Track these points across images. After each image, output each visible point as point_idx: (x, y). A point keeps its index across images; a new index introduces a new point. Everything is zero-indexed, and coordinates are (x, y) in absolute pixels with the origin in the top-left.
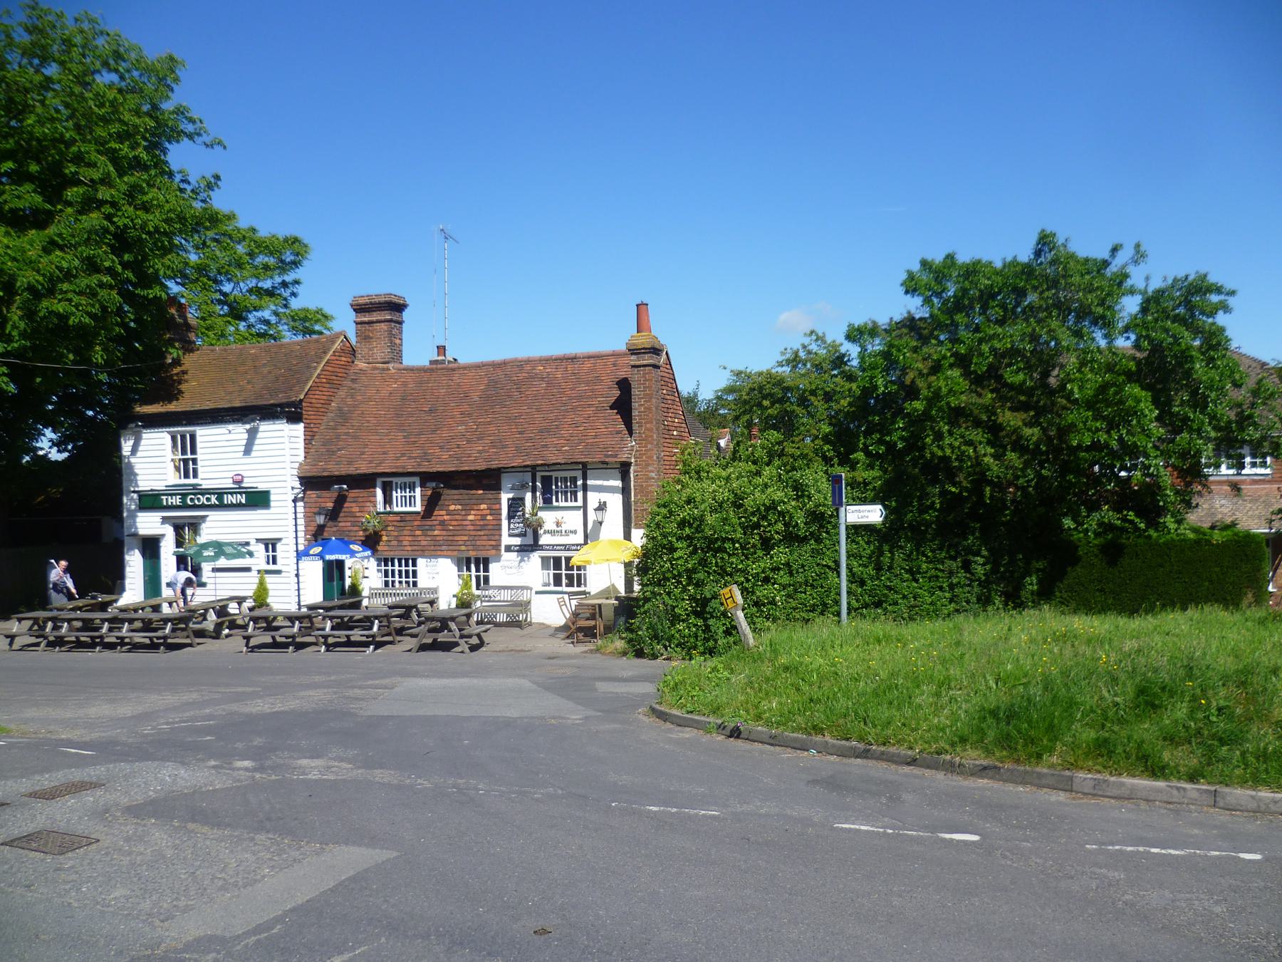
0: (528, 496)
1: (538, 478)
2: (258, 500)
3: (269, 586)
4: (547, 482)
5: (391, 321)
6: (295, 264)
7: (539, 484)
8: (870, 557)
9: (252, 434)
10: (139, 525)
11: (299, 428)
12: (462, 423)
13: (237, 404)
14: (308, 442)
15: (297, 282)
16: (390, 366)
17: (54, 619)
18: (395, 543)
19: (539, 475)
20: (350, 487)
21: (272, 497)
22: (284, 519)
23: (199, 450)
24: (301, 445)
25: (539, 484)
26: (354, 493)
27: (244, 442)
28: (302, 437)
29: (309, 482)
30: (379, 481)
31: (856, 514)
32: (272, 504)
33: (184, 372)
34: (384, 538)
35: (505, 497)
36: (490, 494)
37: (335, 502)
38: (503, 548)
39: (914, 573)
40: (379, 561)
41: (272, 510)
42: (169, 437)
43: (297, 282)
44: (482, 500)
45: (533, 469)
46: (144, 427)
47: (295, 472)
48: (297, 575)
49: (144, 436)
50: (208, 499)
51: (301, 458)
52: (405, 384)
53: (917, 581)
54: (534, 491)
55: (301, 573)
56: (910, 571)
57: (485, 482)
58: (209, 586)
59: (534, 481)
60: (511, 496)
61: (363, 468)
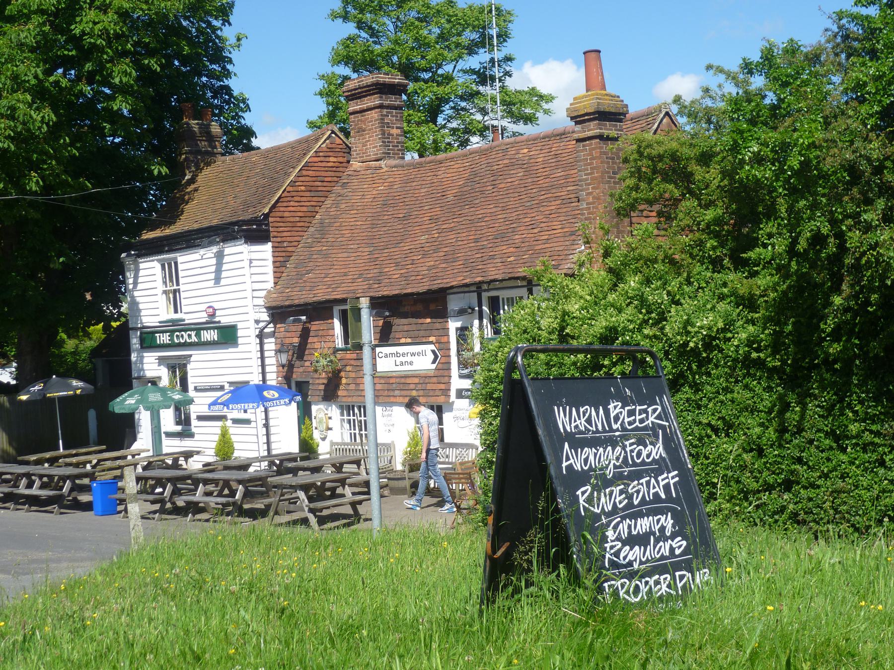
0: (476, 322)
1: (485, 301)
2: (228, 336)
3: (234, 438)
4: (495, 305)
5: (381, 107)
6: (503, 36)
7: (485, 308)
8: (770, 412)
9: (220, 256)
10: (146, 367)
11: (266, 250)
12: (428, 231)
13: (215, 222)
14: (279, 266)
15: (508, 59)
16: (382, 163)
17: (28, 475)
18: (352, 387)
19: (485, 295)
20: (311, 319)
21: (240, 333)
22: (248, 361)
23: (181, 281)
24: (270, 268)
25: (485, 308)
26: (315, 326)
27: (213, 269)
28: (271, 259)
29: (279, 313)
30: (336, 310)
31: (391, 360)
32: (240, 341)
33: (196, 190)
34: (344, 381)
35: (453, 325)
36: (438, 324)
37: (301, 336)
38: (453, 393)
39: (839, 438)
40: (341, 408)
41: (241, 348)
42: (158, 266)
43: (508, 59)
44: (430, 331)
45: (478, 288)
46: (139, 256)
47: (261, 302)
48: (267, 426)
49: (142, 266)
50: (190, 336)
51: (270, 285)
52: (391, 186)
53: (844, 450)
54: (481, 319)
55: (271, 423)
56: (831, 434)
57: (432, 307)
58: (197, 437)
59: (480, 306)
60: (459, 324)
61: (321, 294)
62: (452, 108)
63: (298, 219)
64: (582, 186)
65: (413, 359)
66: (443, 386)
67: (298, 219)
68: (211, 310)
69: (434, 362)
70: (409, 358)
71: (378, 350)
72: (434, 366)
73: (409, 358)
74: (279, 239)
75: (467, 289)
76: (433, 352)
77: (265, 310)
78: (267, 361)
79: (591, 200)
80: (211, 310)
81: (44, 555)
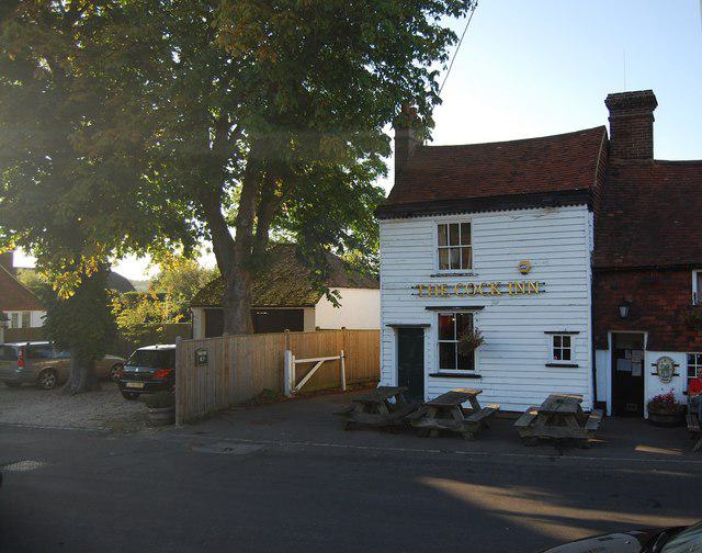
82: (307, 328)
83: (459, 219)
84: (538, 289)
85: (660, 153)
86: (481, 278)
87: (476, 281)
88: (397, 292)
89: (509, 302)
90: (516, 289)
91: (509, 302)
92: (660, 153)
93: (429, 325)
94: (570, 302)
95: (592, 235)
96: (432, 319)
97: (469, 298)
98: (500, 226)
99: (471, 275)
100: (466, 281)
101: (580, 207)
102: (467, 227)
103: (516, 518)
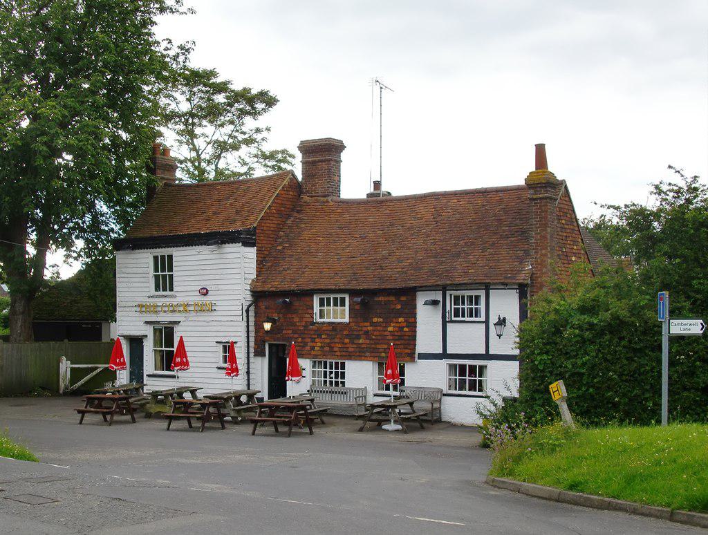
24: (254, 265)
62: (45, 143)
63: (271, 232)
64: (532, 228)
65: (690, 327)
66: (409, 351)
67: (271, 232)
68: (205, 291)
69: (702, 330)
70: (688, 327)
71: (671, 321)
72: (702, 332)
73: (688, 327)
74: (260, 245)
75: (433, 288)
76: (701, 324)
77: (249, 293)
78: (250, 329)
79: (539, 237)
80: (205, 291)
81: (101, 457)
82: (105, 339)
83: (164, 251)
84: (211, 308)
85: (441, 352)
86: (178, 299)
87: (174, 301)
88: (128, 309)
89: (196, 318)
90: (171, 309)
91: (196, 318)
92: (441, 352)
93: (146, 336)
94: (232, 318)
95: (287, 289)
96: (149, 331)
97: (170, 315)
98: (188, 258)
99: (172, 296)
100: (167, 301)
101: (237, 244)
102: (170, 257)
103: (503, 287)
